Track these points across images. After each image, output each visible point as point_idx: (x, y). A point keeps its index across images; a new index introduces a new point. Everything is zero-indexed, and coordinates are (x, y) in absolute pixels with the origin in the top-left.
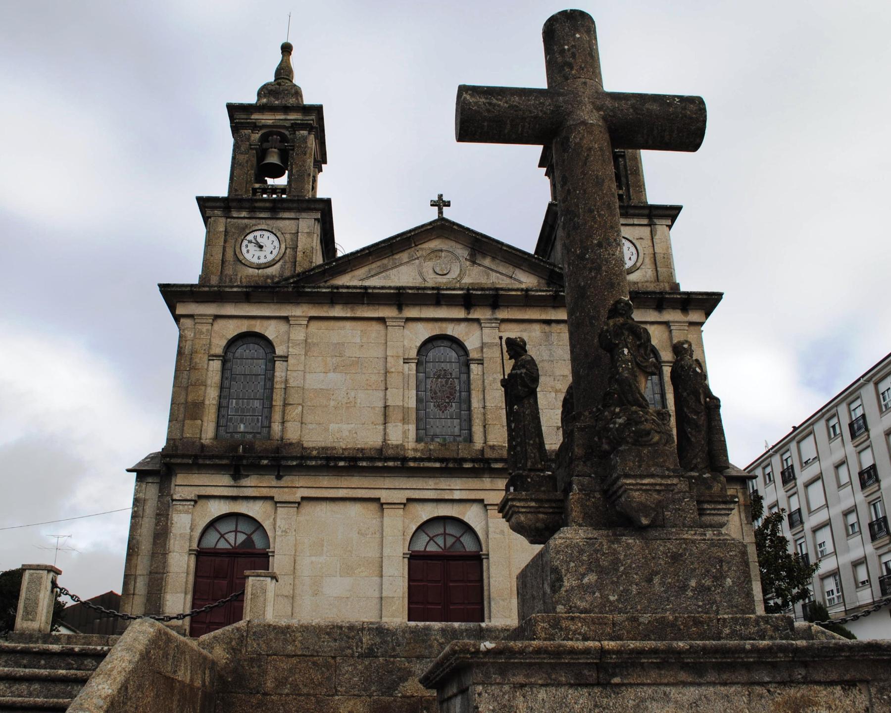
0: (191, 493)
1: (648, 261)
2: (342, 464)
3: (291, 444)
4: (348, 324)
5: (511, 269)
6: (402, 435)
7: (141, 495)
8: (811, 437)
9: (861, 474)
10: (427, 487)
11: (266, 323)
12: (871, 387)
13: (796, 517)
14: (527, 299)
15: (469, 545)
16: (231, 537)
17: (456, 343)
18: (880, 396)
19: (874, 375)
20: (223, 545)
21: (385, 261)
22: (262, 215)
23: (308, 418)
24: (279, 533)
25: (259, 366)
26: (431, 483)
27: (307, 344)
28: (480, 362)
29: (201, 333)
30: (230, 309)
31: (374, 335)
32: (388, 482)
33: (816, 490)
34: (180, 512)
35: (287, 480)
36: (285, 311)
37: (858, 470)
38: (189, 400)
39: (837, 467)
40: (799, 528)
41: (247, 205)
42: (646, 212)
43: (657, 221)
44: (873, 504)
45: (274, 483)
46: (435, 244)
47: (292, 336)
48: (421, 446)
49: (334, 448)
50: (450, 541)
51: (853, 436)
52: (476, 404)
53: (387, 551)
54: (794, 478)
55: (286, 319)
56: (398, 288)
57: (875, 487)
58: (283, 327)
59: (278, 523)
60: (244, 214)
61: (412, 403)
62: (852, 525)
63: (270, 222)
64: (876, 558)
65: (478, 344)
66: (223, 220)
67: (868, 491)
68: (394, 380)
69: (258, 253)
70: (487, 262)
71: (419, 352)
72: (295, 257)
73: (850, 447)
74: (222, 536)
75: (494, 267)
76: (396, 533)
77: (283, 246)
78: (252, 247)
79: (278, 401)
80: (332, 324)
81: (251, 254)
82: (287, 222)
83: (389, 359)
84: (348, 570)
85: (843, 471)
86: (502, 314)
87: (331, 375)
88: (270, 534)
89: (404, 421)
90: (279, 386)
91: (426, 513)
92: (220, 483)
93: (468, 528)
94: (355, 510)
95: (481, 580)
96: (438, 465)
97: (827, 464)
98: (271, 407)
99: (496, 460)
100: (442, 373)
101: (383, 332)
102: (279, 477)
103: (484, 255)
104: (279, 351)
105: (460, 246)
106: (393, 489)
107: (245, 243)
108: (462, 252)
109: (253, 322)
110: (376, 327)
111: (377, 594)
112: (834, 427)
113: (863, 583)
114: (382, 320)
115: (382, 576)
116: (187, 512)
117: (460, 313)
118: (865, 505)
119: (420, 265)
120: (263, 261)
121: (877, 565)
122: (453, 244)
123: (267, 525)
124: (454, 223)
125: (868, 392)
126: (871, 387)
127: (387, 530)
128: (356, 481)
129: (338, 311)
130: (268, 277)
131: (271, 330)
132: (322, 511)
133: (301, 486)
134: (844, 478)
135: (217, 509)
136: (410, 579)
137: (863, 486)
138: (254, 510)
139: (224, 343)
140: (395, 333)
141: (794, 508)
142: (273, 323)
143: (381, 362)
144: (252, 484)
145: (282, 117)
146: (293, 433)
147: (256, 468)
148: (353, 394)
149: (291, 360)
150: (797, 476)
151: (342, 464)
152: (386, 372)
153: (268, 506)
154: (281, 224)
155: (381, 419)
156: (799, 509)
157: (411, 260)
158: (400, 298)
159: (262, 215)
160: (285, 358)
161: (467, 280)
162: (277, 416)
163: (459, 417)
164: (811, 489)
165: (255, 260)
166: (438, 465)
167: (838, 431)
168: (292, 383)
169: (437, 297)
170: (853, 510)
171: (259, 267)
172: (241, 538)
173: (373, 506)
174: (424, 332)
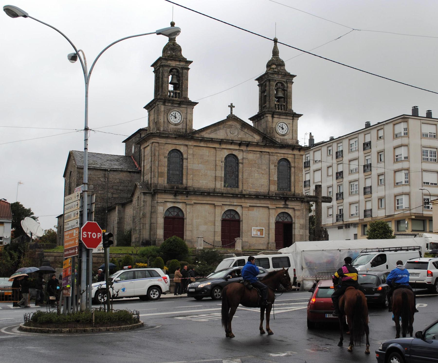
0: (163, 200)
1: (291, 132)
2: (206, 194)
3: (190, 187)
4: (205, 148)
5: (253, 133)
6: (220, 186)
7: (145, 200)
8: (320, 151)
9: (337, 173)
10: (227, 201)
11: (180, 146)
12: (347, 140)
13: (307, 183)
14: (257, 145)
15: (237, 218)
16: (173, 213)
17: (235, 157)
18: (350, 145)
19: (349, 136)
20: (170, 215)
21: (216, 128)
22: (176, 105)
23: (194, 178)
24: (187, 213)
25: (178, 160)
26: (228, 200)
27: (193, 155)
28: (242, 163)
29: (161, 149)
30: (169, 141)
31: (212, 153)
32: (217, 199)
33: (318, 174)
34: (160, 206)
35: (189, 197)
36: (187, 143)
37: (336, 171)
38: (160, 171)
39: (328, 167)
40: (308, 188)
41: (171, 102)
42: (292, 115)
43: (295, 118)
44: (339, 186)
45: (186, 198)
46: (230, 123)
47: (189, 152)
48: (225, 188)
49: (201, 188)
50: (232, 216)
51: (337, 157)
52: (240, 176)
53: (216, 219)
54: (309, 167)
55: (187, 145)
56: (221, 139)
57: (341, 180)
58: (186, 148)
59: (188, 210)
60: (170, 105)
61: (223, 175)
62: (330, 192)
63: (178, 108)
64: (337, 207)
65: (242, 158)
66: (163, 106)
67: (339, 181)
68: (219, 168)
69: (175, 120)
70: (246, 130)
71: (225, 159)
72: (187, 122)
73: (335, 161)
74: (170, 213)
75: (247, 132)
76: (219, 213)
77: (183, 118)
78: (173, 117)
79: (184, 173)
80: (200, 148)
81: (172, 120)
82: (183, 109)
83: (217, 161)
84: (206, 224)
85: (330, 169)
86: (249, 149)
87: (200, 165)
88: (185, 213)
89: (221, 181)
90: (184, 167)
91: (226, 208)
92: (170, 198)
93: (237, 213)
94: (207, 207)
95: (239, 227)
96: (231, 195)
97: (324, 165)
98: (182, 174)
99: (247, 195)
100: (232, 166)
101: (215, 152)
102: (187, 197)
103: (245, 128)
104: (185, 156)
105: (238, 124)
106: (218, 201)
107: (170, 115)
108: (239, 126)
109: (176, 146)
110: (213, 150)
111: (213, 230)
112: (330, 150)
113: (330, 215)
114: (215, 148)
115: (215, 225)
116: (162, 206)
117: (237, 147)
118: (336, 186)
119: (226, 130)
120: (176, 122)
121: (336, 210)
122: (236, 123)
123: (183, 210)
124: (238, 118)
125: (346, 142)
126: (347, 140)
127: (216, 213)
128: (208, 198)
129: (202, 144)
130: (178, 129)
131: (182, 149)
132: (199, 207)
133: (193, 199)
134: (330, 173)
135: (169, 205)
136: (222, 227)
137: (337, 178)
138: (180, 206)
139: (168, 152)
140: (219, 153)
141: (307, 179)
142: (182, 146)
143: (214, 162)
144: (180, 198)
145: (178, 64)
146: (190, 184)
147: (181, 193)
148: (206, 171)
149: (189, 160)
150: (311, 166)
151: (206, 194)
152: (216, 165)
153: (184, 205)
154: (182, 109)
155: (214, 180)
156: (309, 180)
157: (224, 127)
158: (221, 142)
159: (176, 105)
160: (187, 159)
161: (240, 136)
162: (184, 177)
163: (235, 179)
164: (316, 173)
165: (174, 122)
166: (231, 195)
167: (331, 153)
168: (189, 167)
169: (232, 142)
170: (331, 186)
171: (176, 125)
172: (176, 213)
173: (213, 206)
174: (226, 153)
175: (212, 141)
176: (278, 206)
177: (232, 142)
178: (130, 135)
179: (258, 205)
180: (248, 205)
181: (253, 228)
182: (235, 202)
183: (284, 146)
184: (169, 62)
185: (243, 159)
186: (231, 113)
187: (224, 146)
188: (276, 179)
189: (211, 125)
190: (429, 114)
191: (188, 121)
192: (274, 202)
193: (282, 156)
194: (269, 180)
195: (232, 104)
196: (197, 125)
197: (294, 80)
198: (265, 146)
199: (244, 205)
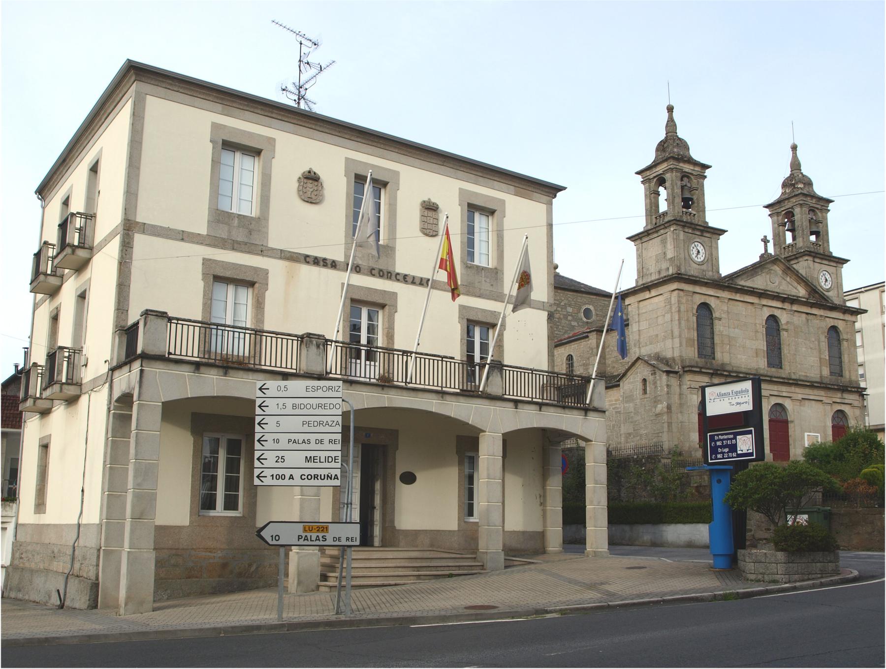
4: (740, 304)
129: (738, 297)
139: (696, 307)
169: (776, 297)
175: (752, 292)
176: (835, 400)
177: (776, 297)
178: (535, 310)
179: (812, 397)
180: (800, 397)
181: (806, 434)
182: (784, 390)
183: (834, 308)
184: (681, 164)
185: (788, 323)
186: (766, 250)
187: (765, 302)
188: (827, 358)
189: (741, 270)
190: (6, 529)
191: (713, 259)
192: (830, 394)
193: (832, 323)
194: (820, 359)
195: (765, 237)
196: (726, 269)
197: (831, 206)
198: (812, 305)
199: (794, 396)
